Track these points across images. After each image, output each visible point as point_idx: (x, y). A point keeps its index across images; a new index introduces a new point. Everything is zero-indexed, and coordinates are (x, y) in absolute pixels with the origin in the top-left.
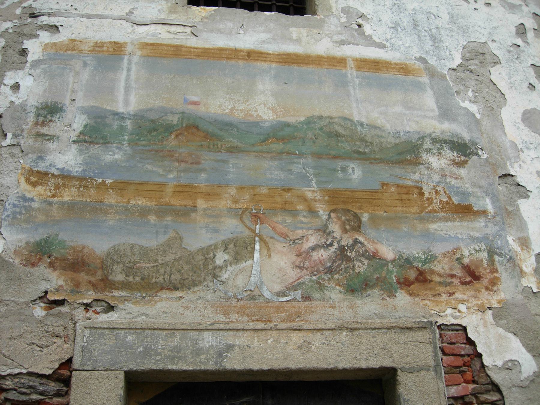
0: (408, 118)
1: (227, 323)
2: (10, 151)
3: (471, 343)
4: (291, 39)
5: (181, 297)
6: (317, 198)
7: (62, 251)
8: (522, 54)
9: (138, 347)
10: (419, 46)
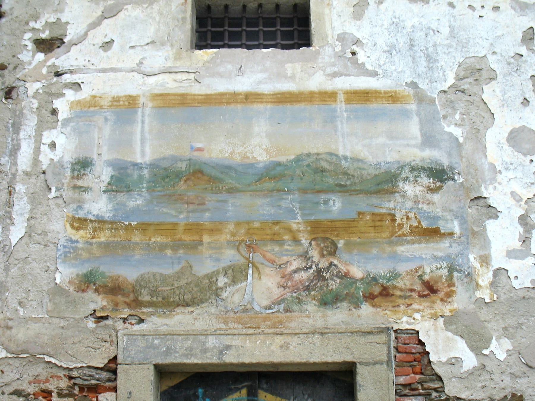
0: (390, 149)
1: (226, 330)
2: (56, 202)
3: (422, 344)
4: (286, 77)
5: (192, 311)
6: (301, 229)
7: (103, 280)
8: (523, 65)
9: (162, 348)
10: (411, 70)
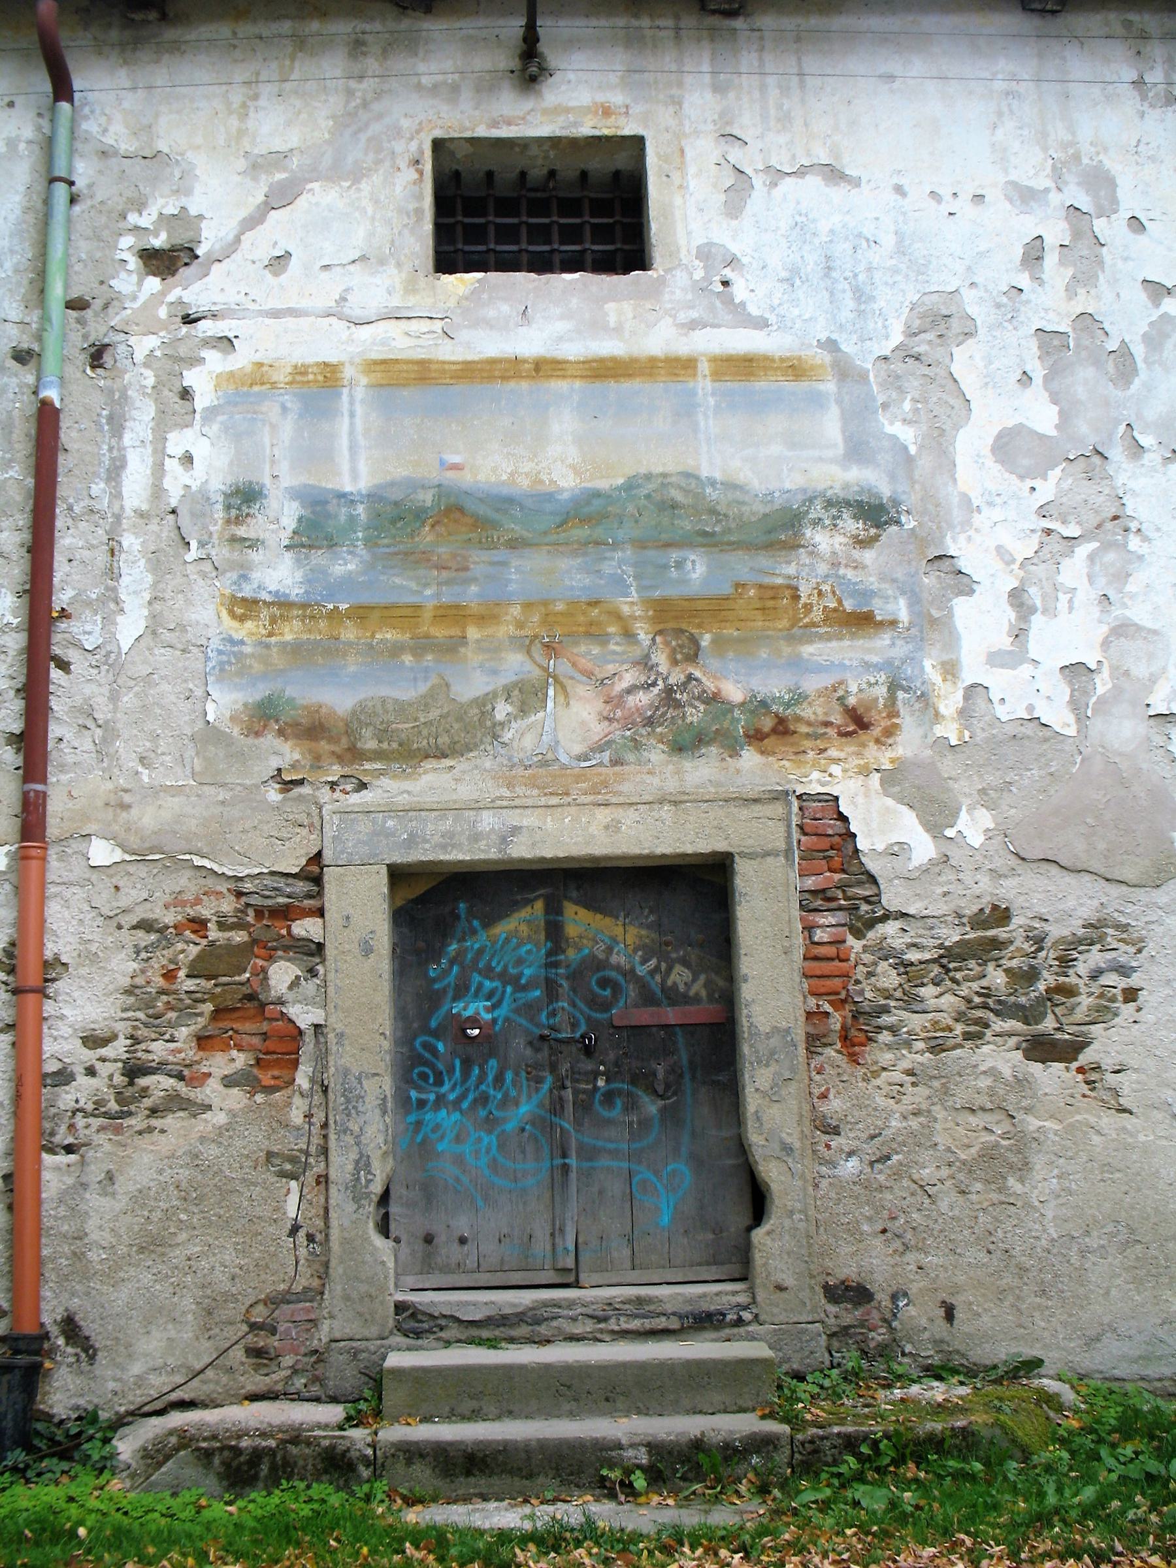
3: (844, 819)
